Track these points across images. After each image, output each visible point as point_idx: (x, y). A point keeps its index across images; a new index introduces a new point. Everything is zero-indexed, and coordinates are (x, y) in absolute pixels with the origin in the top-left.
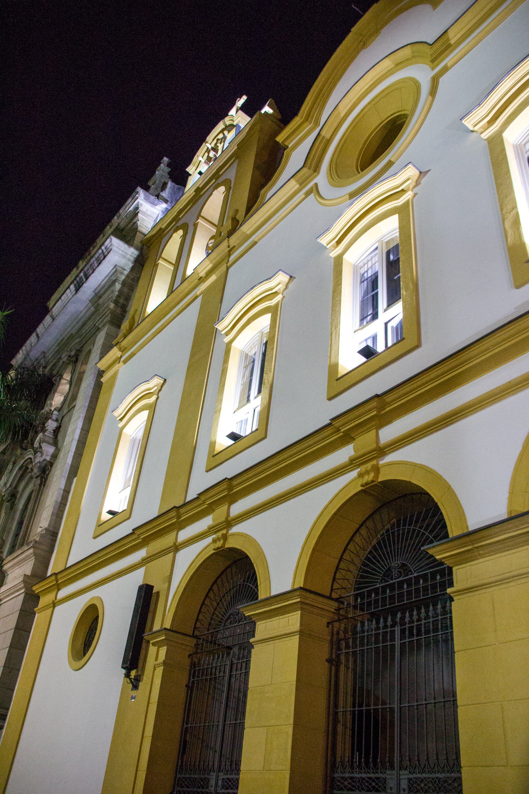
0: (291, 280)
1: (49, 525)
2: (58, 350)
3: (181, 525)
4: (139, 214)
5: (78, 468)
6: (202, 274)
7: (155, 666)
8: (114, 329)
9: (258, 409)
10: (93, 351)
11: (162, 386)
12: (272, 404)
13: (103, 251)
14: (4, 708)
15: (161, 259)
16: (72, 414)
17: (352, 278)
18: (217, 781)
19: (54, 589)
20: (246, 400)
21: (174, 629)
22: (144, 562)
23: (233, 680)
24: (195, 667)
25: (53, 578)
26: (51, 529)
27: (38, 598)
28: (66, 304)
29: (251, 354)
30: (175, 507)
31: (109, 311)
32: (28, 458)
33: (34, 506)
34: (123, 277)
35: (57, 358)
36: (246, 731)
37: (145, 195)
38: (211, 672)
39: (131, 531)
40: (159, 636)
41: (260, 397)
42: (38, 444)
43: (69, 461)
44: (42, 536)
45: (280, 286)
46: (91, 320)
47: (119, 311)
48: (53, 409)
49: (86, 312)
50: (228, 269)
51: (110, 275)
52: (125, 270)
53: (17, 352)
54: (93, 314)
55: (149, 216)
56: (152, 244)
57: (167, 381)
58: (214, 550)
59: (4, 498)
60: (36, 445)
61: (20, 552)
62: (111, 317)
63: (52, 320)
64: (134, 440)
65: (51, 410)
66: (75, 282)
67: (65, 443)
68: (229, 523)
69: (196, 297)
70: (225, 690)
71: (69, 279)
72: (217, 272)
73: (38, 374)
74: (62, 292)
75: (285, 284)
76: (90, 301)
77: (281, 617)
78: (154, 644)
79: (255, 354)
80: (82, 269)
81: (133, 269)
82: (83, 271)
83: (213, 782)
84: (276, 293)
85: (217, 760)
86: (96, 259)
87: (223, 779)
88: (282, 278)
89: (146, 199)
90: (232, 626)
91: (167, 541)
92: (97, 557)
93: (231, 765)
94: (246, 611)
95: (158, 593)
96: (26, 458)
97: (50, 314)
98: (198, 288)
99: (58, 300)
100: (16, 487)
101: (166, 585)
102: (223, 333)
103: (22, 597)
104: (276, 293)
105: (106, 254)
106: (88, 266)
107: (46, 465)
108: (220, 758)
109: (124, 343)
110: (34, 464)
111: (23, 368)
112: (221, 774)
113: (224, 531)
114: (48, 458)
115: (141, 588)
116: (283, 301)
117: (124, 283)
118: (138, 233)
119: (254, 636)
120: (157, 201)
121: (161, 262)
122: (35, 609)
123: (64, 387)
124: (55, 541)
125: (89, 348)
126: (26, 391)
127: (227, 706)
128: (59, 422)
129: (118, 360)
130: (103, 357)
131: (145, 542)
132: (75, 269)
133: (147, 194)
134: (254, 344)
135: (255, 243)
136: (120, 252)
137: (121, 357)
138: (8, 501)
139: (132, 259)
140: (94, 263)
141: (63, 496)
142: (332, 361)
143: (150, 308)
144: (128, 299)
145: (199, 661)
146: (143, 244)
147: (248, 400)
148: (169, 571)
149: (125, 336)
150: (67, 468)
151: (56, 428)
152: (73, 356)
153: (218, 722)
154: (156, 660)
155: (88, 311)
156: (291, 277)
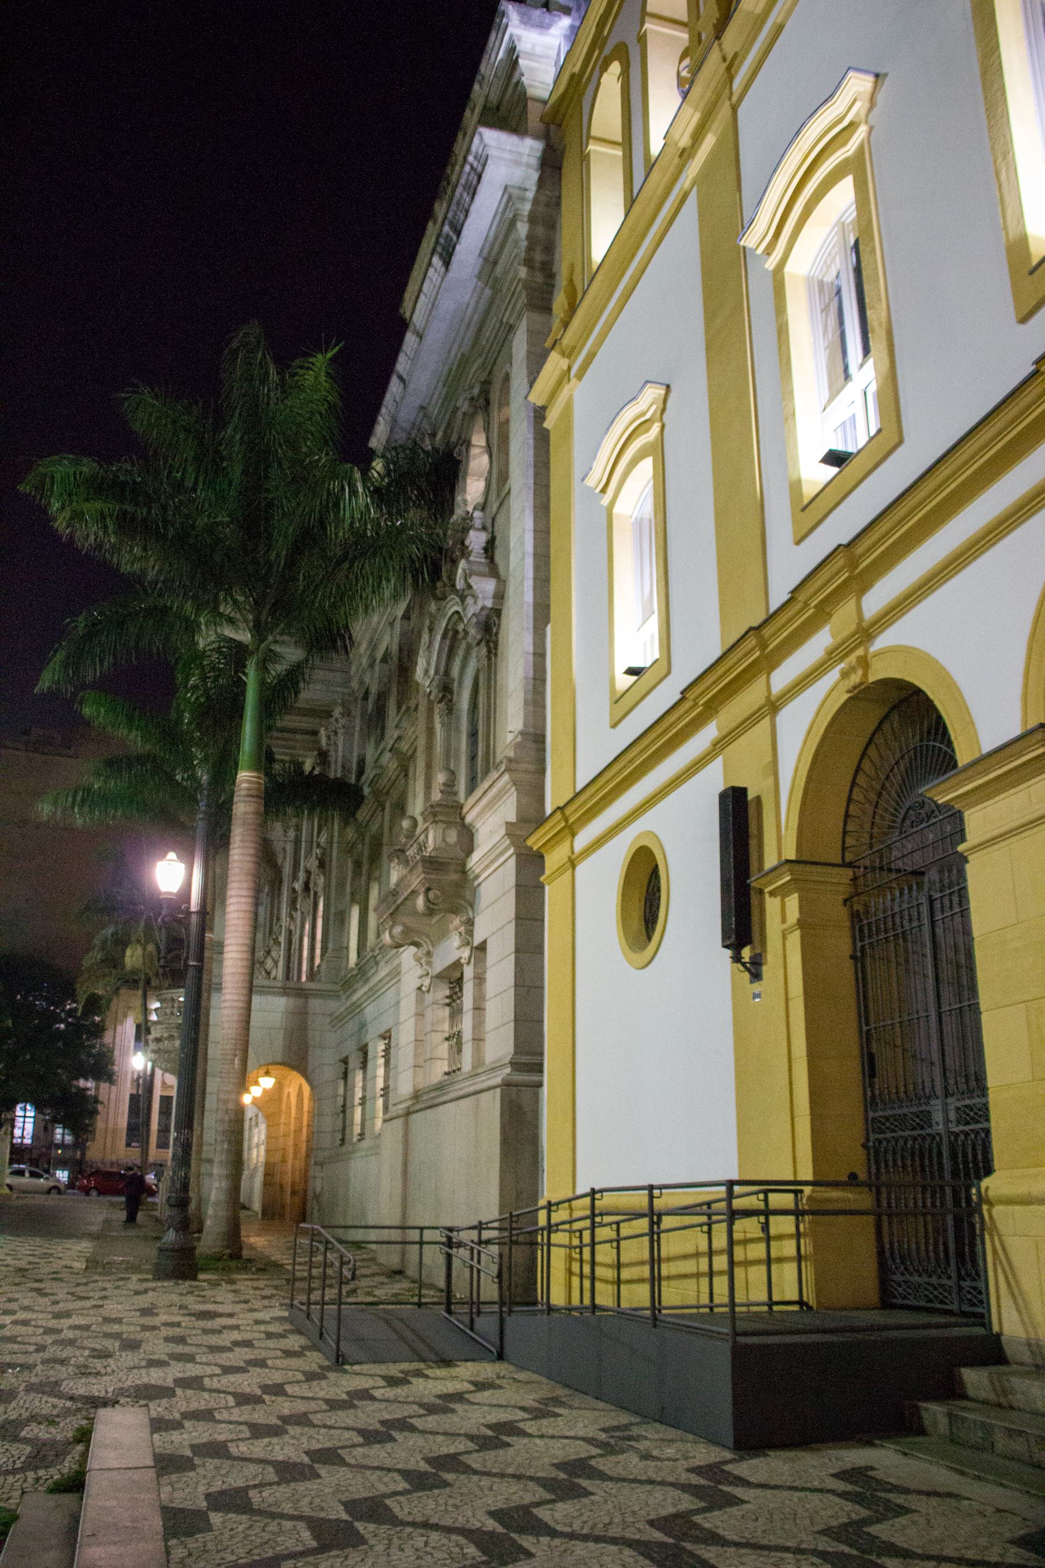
0: (880, 81)
1: (525, 725)
2: (447, 393)
3: (769, 662)
4: (521, 61)
5: (548, 606)
6: (685, 141)
7: (783, 932)
8: (538, 317)
9: (873, 388)
10: (513, 375)
11: (665, 401)
12: (899, 371)
13: (472, 166)
14: (533, 1054)
15: (591, 141)
16: (509, 508)
17: (1021, 22)
18: (946, 1112)
19: (565, 836)
20: (843, 376)
21: (805, 858)
22: (719, 746)
23: (939, 931)
24: (861, 921)
25: (558, 815)
26: (531, 730)
27: (541, 857)
28: (435, 299)
29: (830, 277)
30: (751, 629)
31: (520, 285)
32: (452, 615)
33: (489, 698)
34: (527, 207)
35: (451, 410)
36: (985, 1018)
37: (519, 13)
38: (894, 924)
39: (679, 696)
40: (779, 877)
41: (870, 362)
42: (462, 582)
43: (529, 597)
44: (518, 746)
45: (858, 105)
46: (492, 313)
47: (539, 278)
48: (470, 509)
49: (478, 302)
50: (734, 109)
51: (500, 210)
52: (526, 190)
53: (373, 421)
54: (492, 302)
55: (541, 57)
56: (564, 116)
57: (672, 387)
58: (848, 691)
59: (432, 698)
60: (460, 584)
61: (486, 785)
62: (527, 295)
63: (418, 339)
64: (639, 524)
65: (468, 513)
66: (439, 249)
67: (512, 566)
68: (866, 633)
69: (685, 196)
70: (928, 951)
71: (427, 244)
72: (714, 126)
73: (423, 450)
74: (421, 278)
75: (867, 96)
76: (479, 277)
77: (1013, 791)
78: (772, 894)
79: (838, 276)
80: (445, 218)
81: (541, 182)
82: (447, 222)
83: (938, 1117)
84: (852, 126)
85: (938, 1078)
86: (464, 188)
87: (958, 1109)
88: (858, 85)
89: (526, 21)
90: (915, 829)
91: (751, 697)
92: (628, 759)
93: (967, 1082)
94: (939, 793)
95: (758, 799)
96: (450, 613)
97: (411, 327)
98: (684, 175)
99: (418, 297)
100: (447, 673)
101: (771, 780)
102: (759, 251)
103: (512, 862)
104: (852, 126)
105: (479, 169)
106: (454, 207)
107: (488, 617)
108: (945, 1075)
109: (567, 340)
110: (466, 621)
111: (395, 448)
112: (950, 1100)
113: (860, 652)
114: (489, 604)
115: (723, 796)
116: (872, 138)
117: (532, 219)
118: (530, 103)
119: (963, 839)
120: (547, 17)
121: (592, 147)
122: (542, 879)
123: (478, 462)
124: (544, 750)
125: (504, 371)
126: (412, 490)
127: (937, 979)
128: (490, 530)
129: (565, 376)
130: (535, 379)
131: (711, 709)
132: (430, 225)
133: (523, 8)
134: (830, 254)
135: (779, 29)
136: (507, 156)
137: (569, 368)
138: (440, 702)
139: (534, 162)
140: (461, 196)
141: (535, 665)
142: (1011, 233)
143: (598, 253)
144: (550, 248)
145: (866, 906)
146: (548, 124)
147: (847, 377)
148: (770, 752)
149: (566, 325)
150: (529, 610)
151: (488, 542)
152: (479, 396)
153: (927, 1010)
154: (784, 920)
155: (480, 298)
156: (877, 76)
